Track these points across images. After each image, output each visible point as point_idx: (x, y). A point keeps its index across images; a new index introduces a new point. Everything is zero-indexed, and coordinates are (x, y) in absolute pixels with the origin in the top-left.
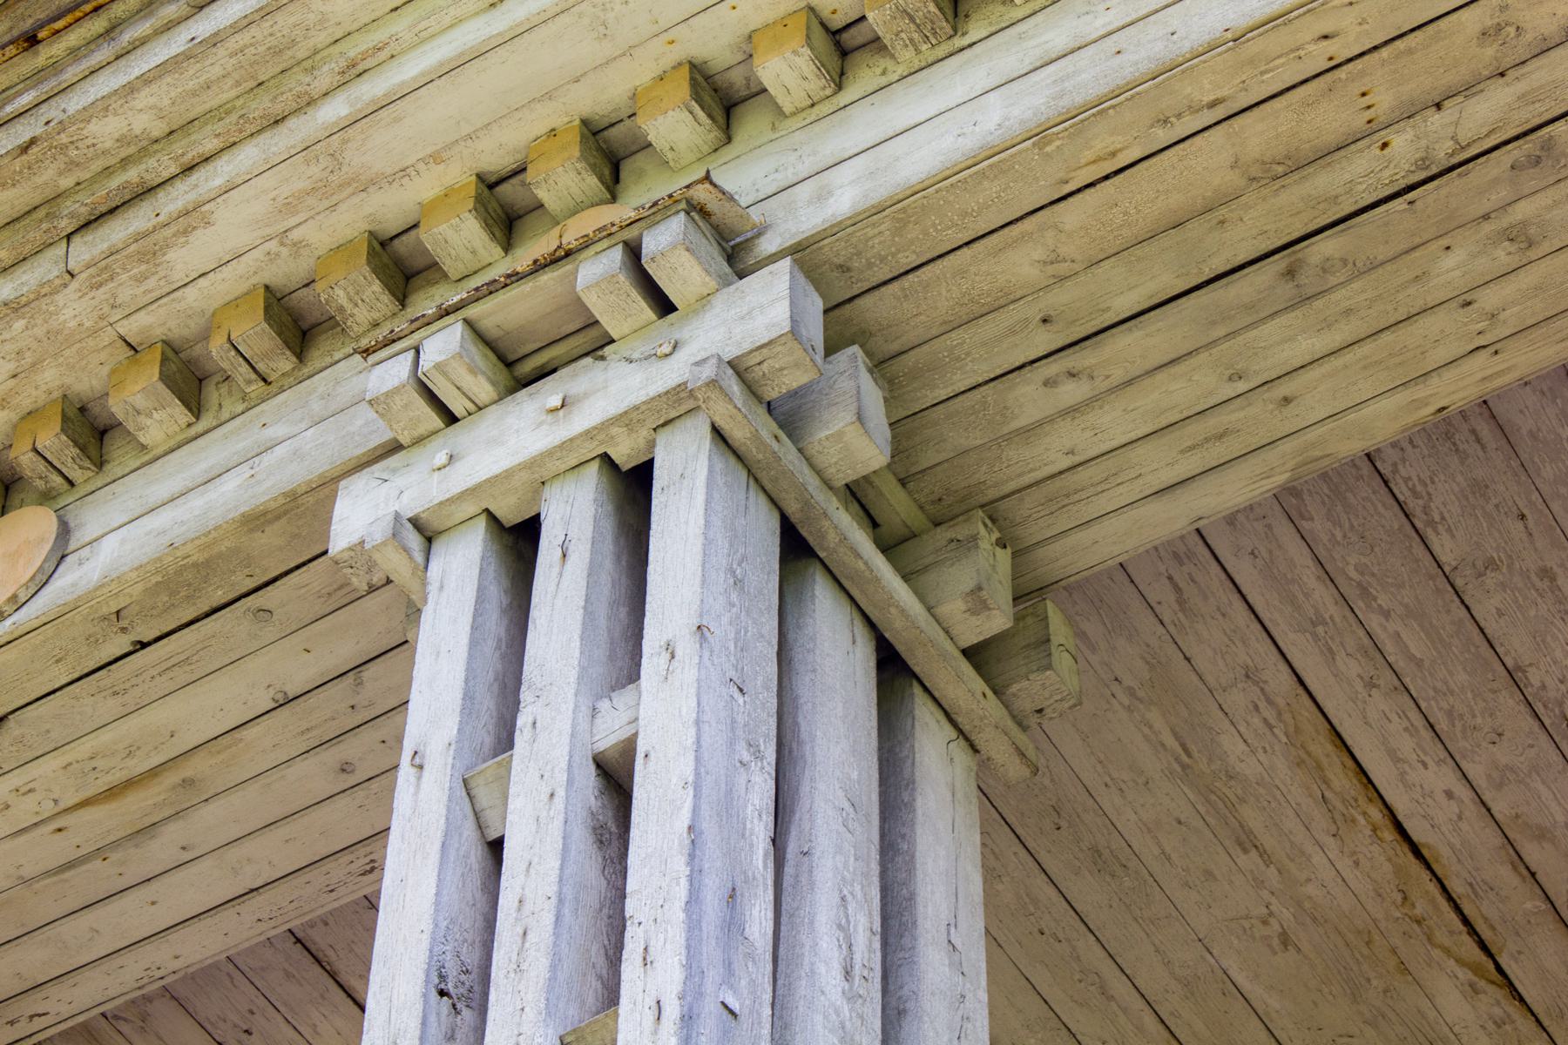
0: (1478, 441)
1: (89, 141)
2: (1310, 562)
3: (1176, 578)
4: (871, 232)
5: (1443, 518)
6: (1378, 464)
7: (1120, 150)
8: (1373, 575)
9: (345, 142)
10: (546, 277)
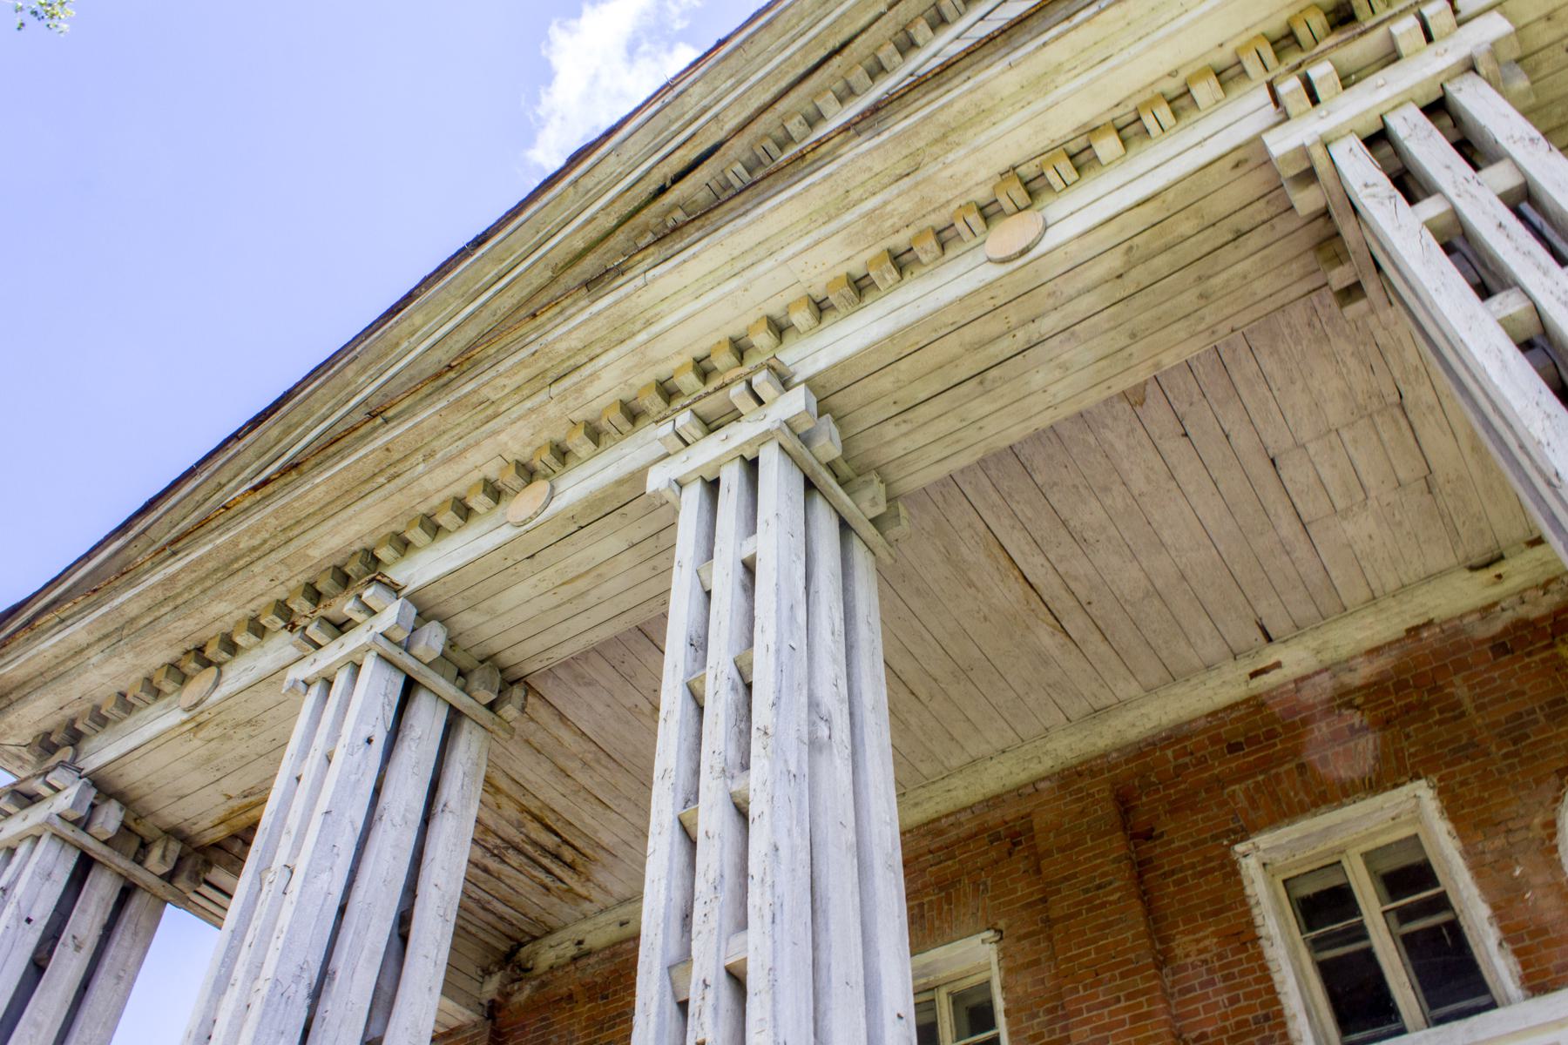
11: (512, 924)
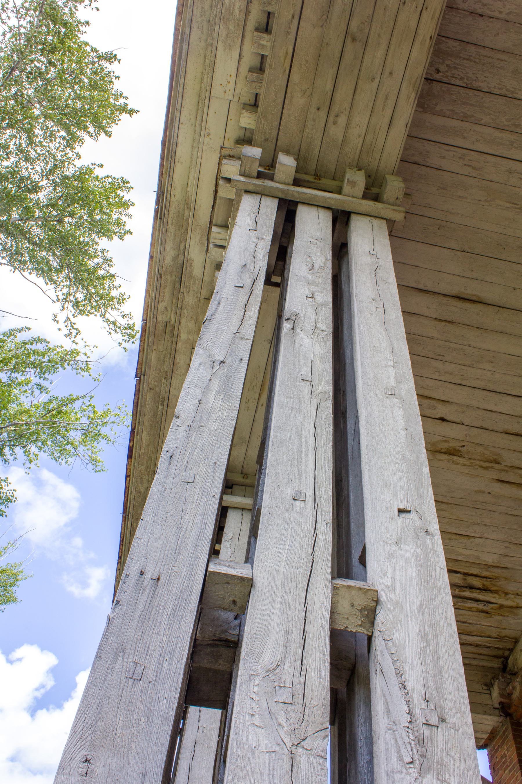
0: (502, 60)
1: (168, 266)
2: (494, 130)
3: (466, 163)
4: (262, 125)
5: (515, 88)
6: (483, 90)
7: (287, 50)
8: (513, 119)
9: (196, 220)
10: (218, 201)
11: (488, 647)
